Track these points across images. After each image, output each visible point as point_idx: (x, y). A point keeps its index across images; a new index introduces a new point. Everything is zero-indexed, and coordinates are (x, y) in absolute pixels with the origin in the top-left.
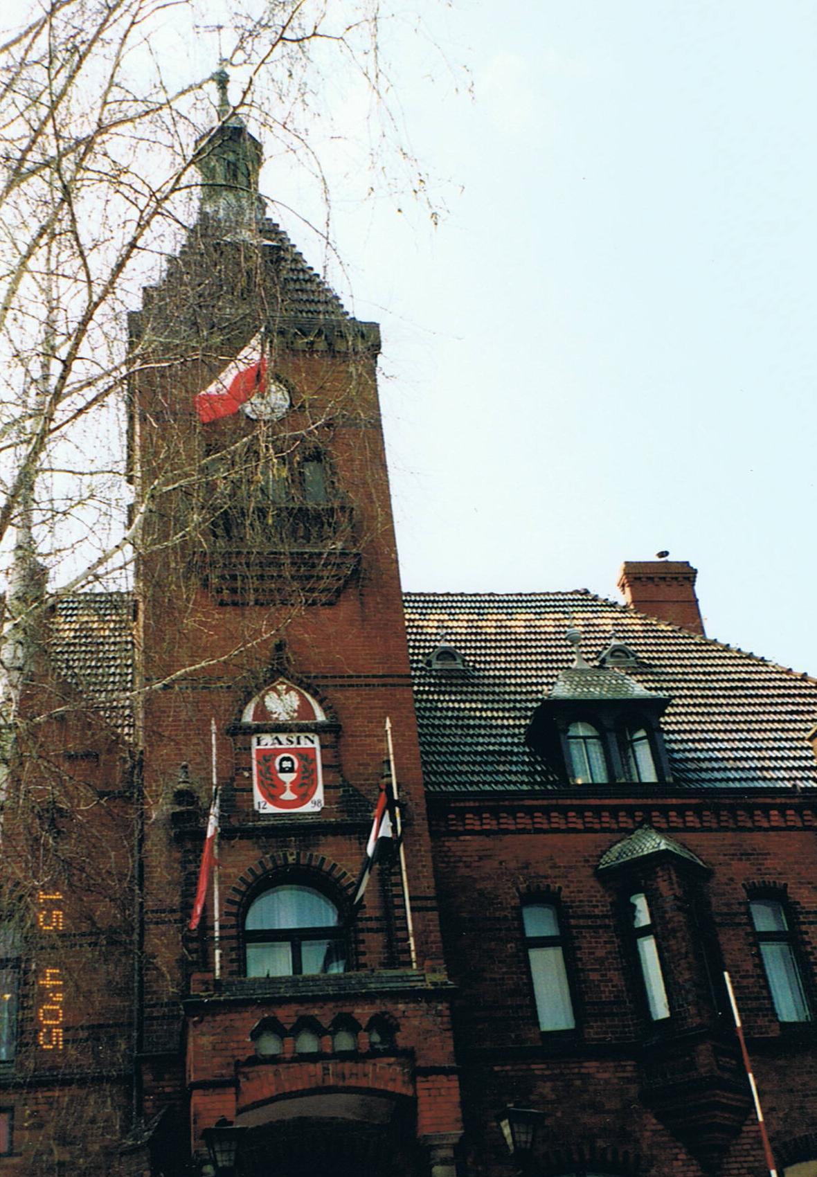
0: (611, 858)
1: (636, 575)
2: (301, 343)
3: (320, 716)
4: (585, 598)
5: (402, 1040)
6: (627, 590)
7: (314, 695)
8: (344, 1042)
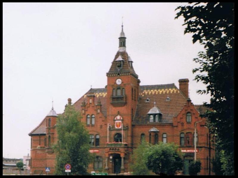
0: (149, 131)
2: (125, 74)
4: (172, 86)
5: (120, 150)
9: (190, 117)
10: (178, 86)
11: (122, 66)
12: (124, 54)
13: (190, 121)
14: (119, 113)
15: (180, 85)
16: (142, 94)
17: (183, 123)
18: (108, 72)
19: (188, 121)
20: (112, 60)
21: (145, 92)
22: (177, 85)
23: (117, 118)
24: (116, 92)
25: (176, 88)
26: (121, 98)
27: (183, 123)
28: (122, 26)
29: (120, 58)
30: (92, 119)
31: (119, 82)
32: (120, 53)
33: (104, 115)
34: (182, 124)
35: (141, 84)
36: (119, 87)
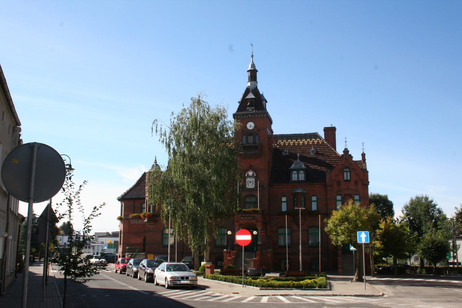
0: (293, 192)
1: (326, 130)
3: (255, 175)
4: (315, 136)
6: (331, 126)
7: (255, 172)
8: (250, 218)
9: (348, 173)
10: (323, 136)
11: (253, 105)
12: (255, 91)
13: (349, 178)
14: (251, 168)
15: (325, 135)
16: (276, 145)
17: (340, 182)
18: (234, 113)
19: (345, 179)
20: (240, 98)
21: (280, 142)
22: (322, 134)
23: (248, 175)
24: (247, 139)
25: (320, 138)
26: (256, 148)
27: (340, 182)
28: (252, 56)
29: (251, 96)
30: (388, 262)
31: (250, 125)
32: (185, 279)
33: (243, 158)
34: (339, 183)
35: (274, 134)
36: (250, 133)
